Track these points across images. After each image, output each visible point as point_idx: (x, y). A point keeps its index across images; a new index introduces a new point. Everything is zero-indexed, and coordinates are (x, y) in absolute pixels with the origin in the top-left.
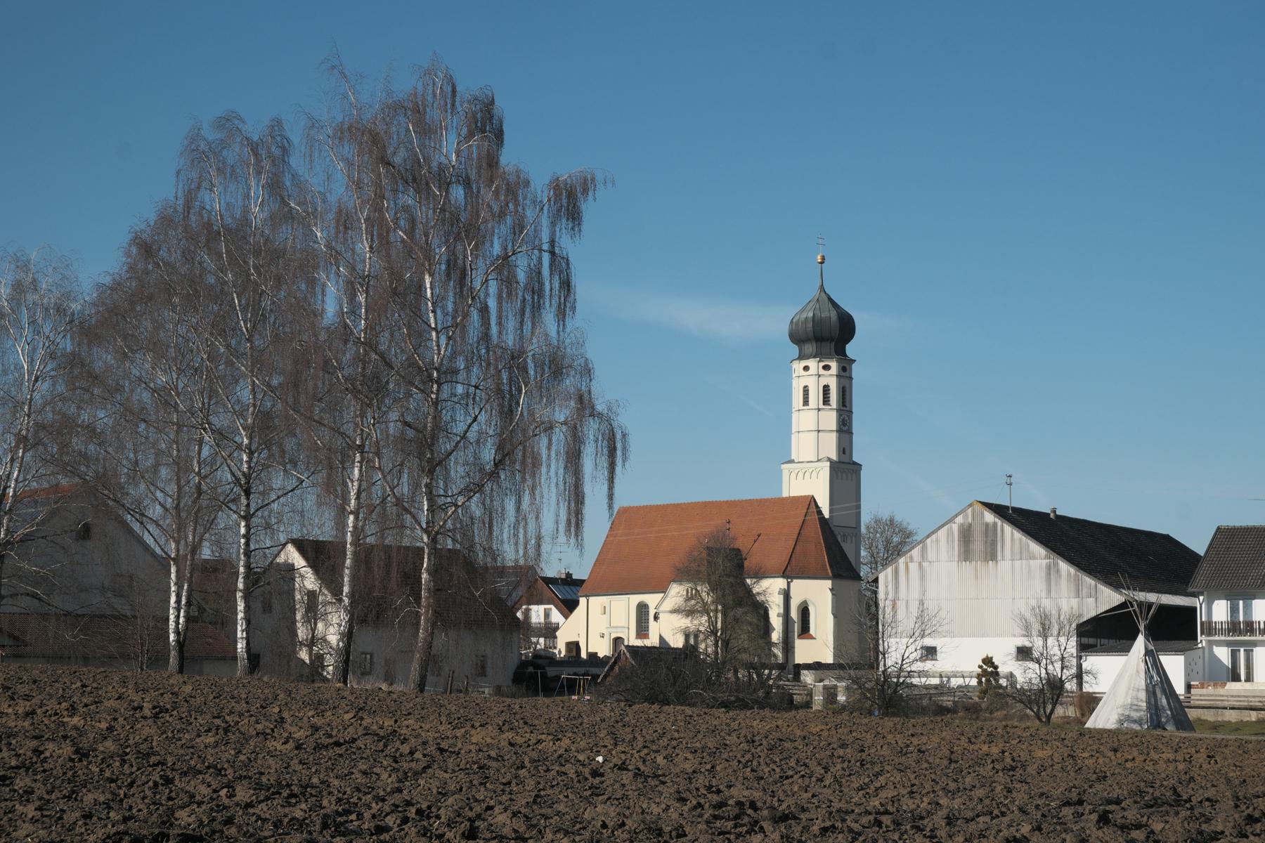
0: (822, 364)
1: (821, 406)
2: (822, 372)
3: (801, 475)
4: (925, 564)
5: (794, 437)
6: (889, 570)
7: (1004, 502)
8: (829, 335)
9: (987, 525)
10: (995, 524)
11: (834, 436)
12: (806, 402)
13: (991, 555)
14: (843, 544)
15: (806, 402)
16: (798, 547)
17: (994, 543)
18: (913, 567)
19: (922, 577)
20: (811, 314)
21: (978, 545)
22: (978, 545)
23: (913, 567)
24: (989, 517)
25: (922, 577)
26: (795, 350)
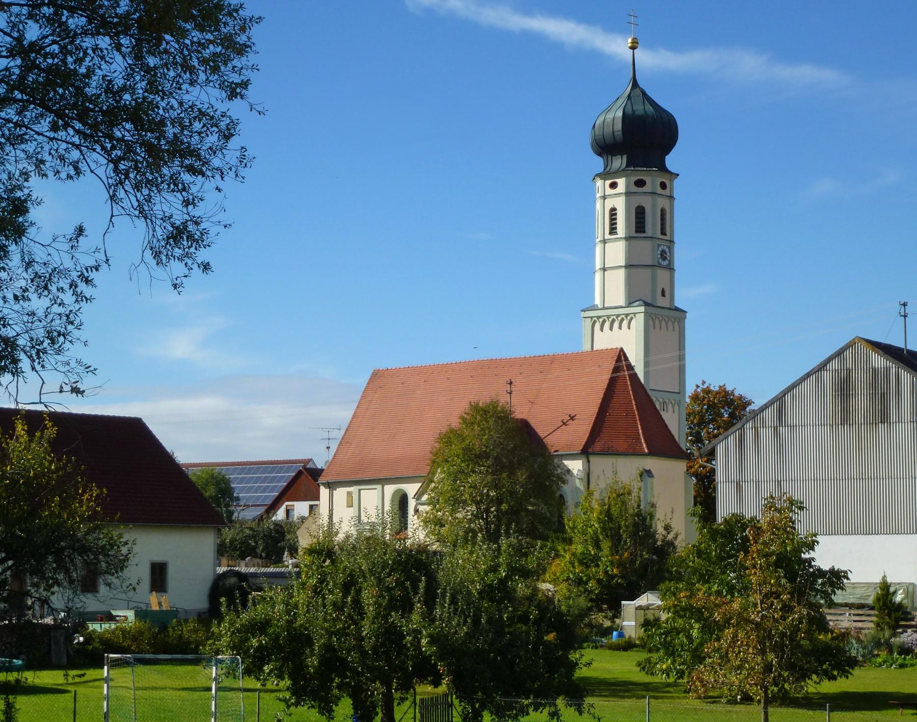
0: (608, 182)
1: (607, 236)
2: (609, 191)
3: (607, 325)
4: (782, 430)
5: (21, 406)
6: (732, 440)
7: (899, 343)
8: (642, 141)
9: (875, 370)
10: (887, 369)
11: (622, 273)
12: (613, 230)
13: (882, 415)
14: (662, 413)
15: (613, 230)
16: (551, 431)
17: (884, 398)
18: (766, 434)
19: (780, 448)
20: (620, 114)
21: (861, 403)
22: (861, 403)
23: (766, 434)
24: (879, 361)
25: (780, 448)
26: (598, 163)
